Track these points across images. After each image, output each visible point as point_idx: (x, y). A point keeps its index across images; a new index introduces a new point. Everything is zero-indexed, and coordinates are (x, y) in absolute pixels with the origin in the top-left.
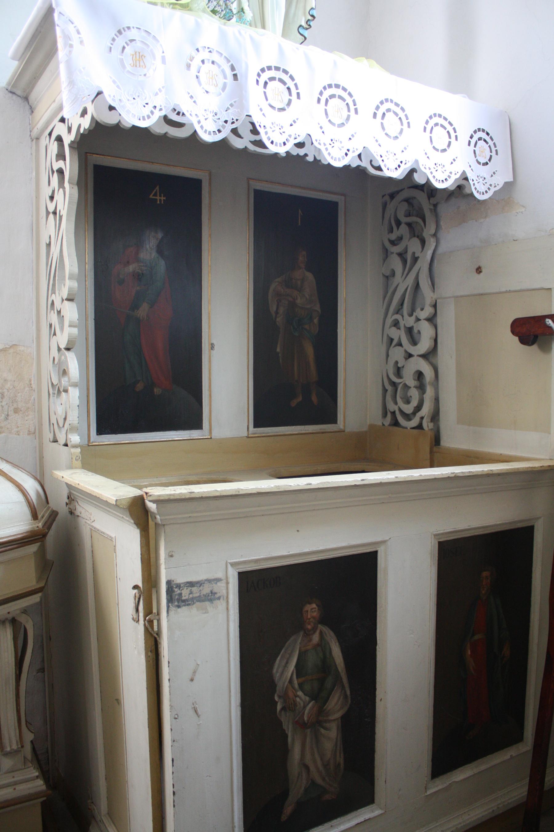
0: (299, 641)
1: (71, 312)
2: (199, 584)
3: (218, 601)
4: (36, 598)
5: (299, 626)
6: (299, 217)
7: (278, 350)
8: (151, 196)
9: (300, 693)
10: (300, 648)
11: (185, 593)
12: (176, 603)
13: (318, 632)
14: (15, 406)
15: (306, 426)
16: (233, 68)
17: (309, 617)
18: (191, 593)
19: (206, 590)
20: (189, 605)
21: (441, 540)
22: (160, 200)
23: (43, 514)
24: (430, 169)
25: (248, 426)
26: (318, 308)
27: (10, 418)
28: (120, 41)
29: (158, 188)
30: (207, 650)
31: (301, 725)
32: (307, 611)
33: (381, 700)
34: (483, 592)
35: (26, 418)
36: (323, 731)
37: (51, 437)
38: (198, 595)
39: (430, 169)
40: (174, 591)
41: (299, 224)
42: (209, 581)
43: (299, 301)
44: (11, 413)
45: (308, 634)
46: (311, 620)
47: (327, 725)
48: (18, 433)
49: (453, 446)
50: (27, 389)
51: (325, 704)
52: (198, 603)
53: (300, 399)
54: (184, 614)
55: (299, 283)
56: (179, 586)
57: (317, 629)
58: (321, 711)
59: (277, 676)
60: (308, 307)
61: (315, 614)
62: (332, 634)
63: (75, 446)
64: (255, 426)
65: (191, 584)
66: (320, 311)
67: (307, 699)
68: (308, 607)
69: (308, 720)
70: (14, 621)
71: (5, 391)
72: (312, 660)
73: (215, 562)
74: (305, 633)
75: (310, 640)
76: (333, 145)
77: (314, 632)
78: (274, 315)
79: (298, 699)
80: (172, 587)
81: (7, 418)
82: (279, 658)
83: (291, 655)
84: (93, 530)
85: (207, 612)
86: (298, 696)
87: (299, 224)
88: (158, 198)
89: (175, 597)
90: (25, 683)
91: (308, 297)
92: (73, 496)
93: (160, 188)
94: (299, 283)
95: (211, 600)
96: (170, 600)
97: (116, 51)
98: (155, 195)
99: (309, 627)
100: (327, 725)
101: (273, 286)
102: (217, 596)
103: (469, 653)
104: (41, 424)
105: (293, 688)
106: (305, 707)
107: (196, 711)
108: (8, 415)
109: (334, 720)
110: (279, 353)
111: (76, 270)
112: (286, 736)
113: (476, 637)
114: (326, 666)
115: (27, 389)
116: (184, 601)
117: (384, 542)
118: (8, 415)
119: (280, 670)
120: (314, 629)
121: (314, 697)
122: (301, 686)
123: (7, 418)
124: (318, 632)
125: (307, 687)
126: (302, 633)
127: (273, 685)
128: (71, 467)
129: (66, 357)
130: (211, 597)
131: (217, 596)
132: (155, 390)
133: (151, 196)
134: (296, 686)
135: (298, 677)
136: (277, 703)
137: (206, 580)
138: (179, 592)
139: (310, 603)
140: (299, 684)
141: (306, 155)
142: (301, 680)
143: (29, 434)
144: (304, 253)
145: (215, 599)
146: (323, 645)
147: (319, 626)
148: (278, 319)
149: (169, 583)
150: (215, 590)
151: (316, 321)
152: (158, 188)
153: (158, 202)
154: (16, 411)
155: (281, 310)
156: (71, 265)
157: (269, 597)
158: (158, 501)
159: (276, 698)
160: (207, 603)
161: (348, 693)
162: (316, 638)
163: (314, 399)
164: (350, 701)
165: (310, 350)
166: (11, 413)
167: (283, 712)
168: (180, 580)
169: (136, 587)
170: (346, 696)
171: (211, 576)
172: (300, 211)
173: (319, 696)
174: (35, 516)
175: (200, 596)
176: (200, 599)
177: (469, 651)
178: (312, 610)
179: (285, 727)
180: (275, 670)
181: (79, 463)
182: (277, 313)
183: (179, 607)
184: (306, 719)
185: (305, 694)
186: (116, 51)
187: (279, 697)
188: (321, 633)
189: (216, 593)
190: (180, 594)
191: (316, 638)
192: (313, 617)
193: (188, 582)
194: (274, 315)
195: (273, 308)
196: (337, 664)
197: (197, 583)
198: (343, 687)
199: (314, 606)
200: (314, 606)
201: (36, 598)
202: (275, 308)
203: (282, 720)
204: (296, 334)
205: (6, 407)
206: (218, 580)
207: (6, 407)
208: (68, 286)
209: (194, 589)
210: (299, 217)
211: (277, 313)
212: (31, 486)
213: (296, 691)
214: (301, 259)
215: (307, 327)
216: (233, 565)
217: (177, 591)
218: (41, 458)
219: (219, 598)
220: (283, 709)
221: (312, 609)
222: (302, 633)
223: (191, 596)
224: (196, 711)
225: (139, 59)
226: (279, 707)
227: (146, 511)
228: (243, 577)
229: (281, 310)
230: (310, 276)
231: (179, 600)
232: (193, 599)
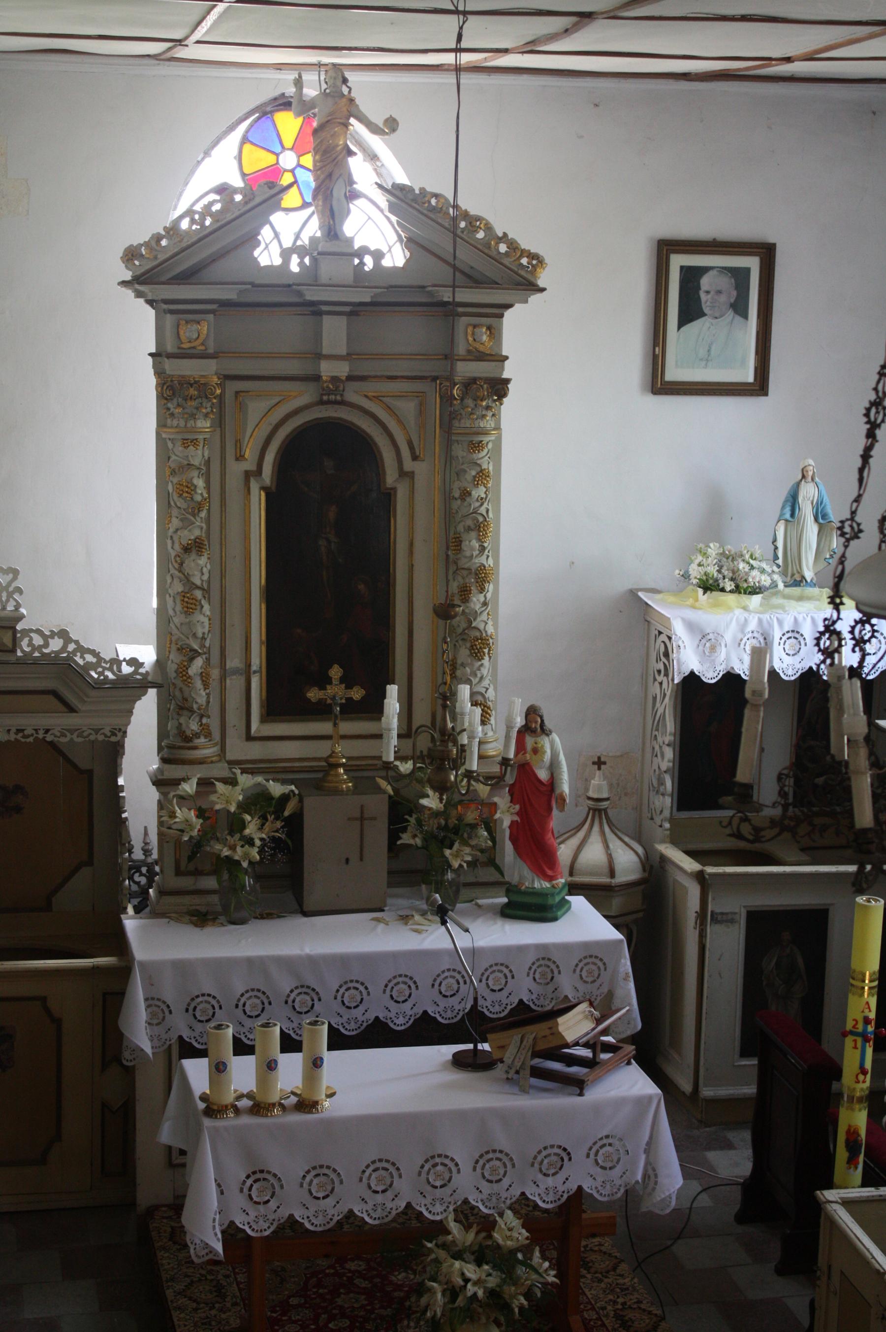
1: (669, 753)
2: (727, 914)
4: (641, 915)
11: (719, 917)
16: (765, 639)
19: (730, 917)
23: (647, 867)
28: (703, 641)
30: (729, 946)
37: (649, 815)
48: (626, 809)
54: (718, 928)
56: (716, 914)
63: (667, 830)
65: (722, 914)
70: (627, 926)
73: (736, 904)
84: (675, 881)
89: (715, 919)
92: (663, 859)
96: (712, 919)
97: (701, 648)
104: (641, 805)
111: (673, 731)
117: (832, 904)
128: (663, 842)
130: (732, 921)
149: (712, 912)
154: (626, 794)
156: (670, 725)
157: (762, 928)
158: (711, 875)
168: (718, 910)
169: (151, 355)
174: (644, 870)
176: (727, 921)
181: (668, 840)
186: (701, 648)
201: (641, 915)
206: (735, 913)
208: (668, 738)
212: (640, 850)
216: (744, 907)
218: (640, 826)
225: (713, 649)
226: (764, 983)
227: (704, 878)
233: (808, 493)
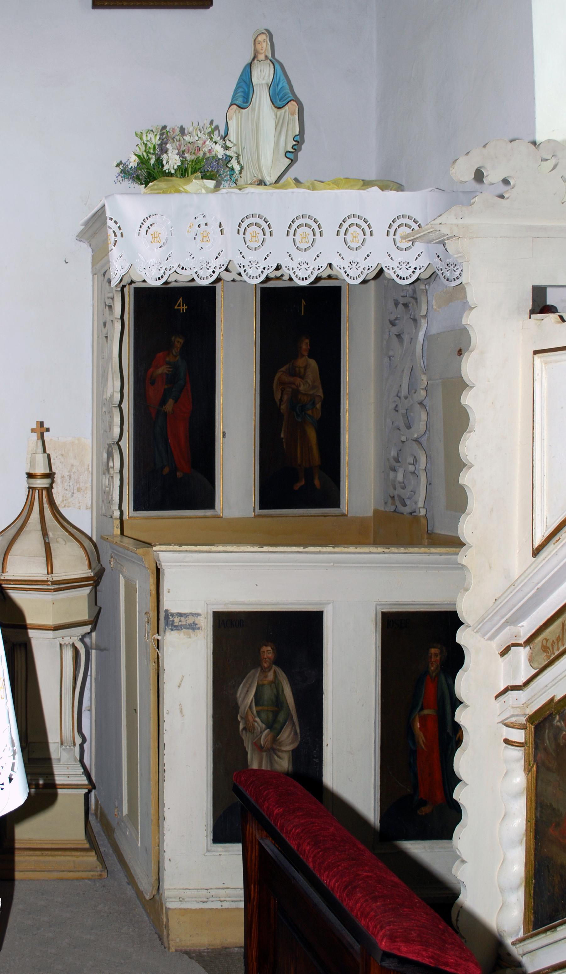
0: (257, 675)
3: (197, 630)
5: (257, 662)
6: (303, 307)
7: (282, 436)
8: (176, 308)
9: (257, 719)
10: (258, 681)
11: (177, 620)
12: (170, 627)
13: (272, 671)
14: (78, 486)
15: (308, 509)
17: (265, 657)
18: (180, 621)
19: (190, 620)
20: (178, 630)
21: (384, 611)
22: (183, 309)
24: (393, 269)
25: (254, 507)
26: (320, 393)
27: (74, 495)
29: (181, 299)
31: (260, 748)
32: (264, 652)
33: (327, 745)
34: (432, 668)
35: (85, 496)
36: (276, 758)
38: (185, 623)
39: (393, 269)
40: (169, 618)
41: (303, 314)
42: (192, 614)
43: (302, 388)
44: (75, 491)
45: (264, 671)
46: (267, 659)
47: (280, 754)
49: (443, 533)
50: (86, 472)
51: (278, 734)
52: (184, 630)
53: (303, 483)
55: (302, 370)
56: (172, 615)
57: (271, 668)
58: (274, 740)
59: (240, 700)
60: (311, 393)
61: (270, 655)
62: (284, 675)
64: (260, 508)
65: (180, 615)
66: (322, 396)
67: (264, 726)
68: (264, 649)
69: (264, 745)
71: (72, 473)
72: (268, 694)
74: (262, 669)
75: (266, 677)
76: (300, 267)
77: (270, 670)
78: (278, 403)
79: (256, 724)
80: (168, 615)
81: (72, 496)
82: (241, 686)
83: (250, 686)
85: (190, 638)
86: (256, 721)
87: (303, 314)
88: (181, 308)
90: (69, 790)
91: (310, 383)
93: (182, 299)
94: (302, 370)
95: (193, 629)
96: (167, 624)
98: (179, 306)
99: (266, 665)
100: (280, 754)
101: (278, 375)
102: (197, 626)
103: (418, 726)
105: (253, 713)
106: (261, 732)
107: (181, 711)
108: (73, 493)
109: (286, 751)
110: (283, 439)
112: (247, 753)
113: (426, 712)
114: (279, 702)
115: (86, 472)
116: (175, 626)
118: (73, 493)
119: (242, 695)
120: (270, 668)
121: (270, 726)
122: (258, 712)
123: (72, 496)
124: (272, 671)
125: (263, 715)
126: (259, 669)
127: (236, 708)
129: (112, 449)
130: (194, 627)
131: (197, 626)
132: (178, 474)
133: (176, 308)
134: (255, 712)
135: (256, 705)
136: (239, 722)
137: (191, 613)
138: (172, 619)
139: (266, 646)
140: (257, 711)
141: (282, 275)
142: (259, 708)
143: (87, 509)
144: (307, 341)
145: (196, 629)
146: (276, 683)
147: (274, 666)
148: (282, 407)
150: (196, 622)
151: (318, 406)
152: (181, 299)
153: (181, 311)
154: (79, 490)
155: (285, 398)
159: (239, 719)
160: (190, 631)
161: (298, 731)
162: (271, 676)
163: (317, 482)
164: (299, 739)
165: (312, 434)
166: (75, 491)
167: (244, 732)
168: (173, 610)
170: (296, 733)
171: (194, 611)
172: (303, 301)
173: (274, 726)
175: (186, 625)
177: (418, 724)
178: (268, 652)
179: (245, 745)
180: (238, 695)
182: (281, 400)
183: (172, 630)
184: (262, 743)
185: (262, 721)
187: (242, 718)
188: (275, 672)
189: (197, 624)
190: (173, 621)
191: (271, 676)
192: (269, 658)
193: (178, 613)
194: (278, 403)
195: (278, 396)
196: (288, 702)
197: (185, 614)
198: (294, 724)
199: (269, 648)
200: (269, 648)
202: (279, 397)
203: (244, 738)
204: (300, 420)
205: (72, 487)
207: (72, 487)
209: (182, 619)
210: (303, 307)
211: (281, 400)
213: (255, 717)
214: (304, 347)
215: (309, 412)
217: (171, 618)
219: (199, 629)
220: (244, 729)
221: (268, 651)
222: (259, 669)
223: (180, 623)
224: (181, 711)
226: (241, 726)
228: (213, 612)
229: (285, 398)
230: (313, 363)
231: (173, 625)
232: (181, 626)
233: (262, 75)
